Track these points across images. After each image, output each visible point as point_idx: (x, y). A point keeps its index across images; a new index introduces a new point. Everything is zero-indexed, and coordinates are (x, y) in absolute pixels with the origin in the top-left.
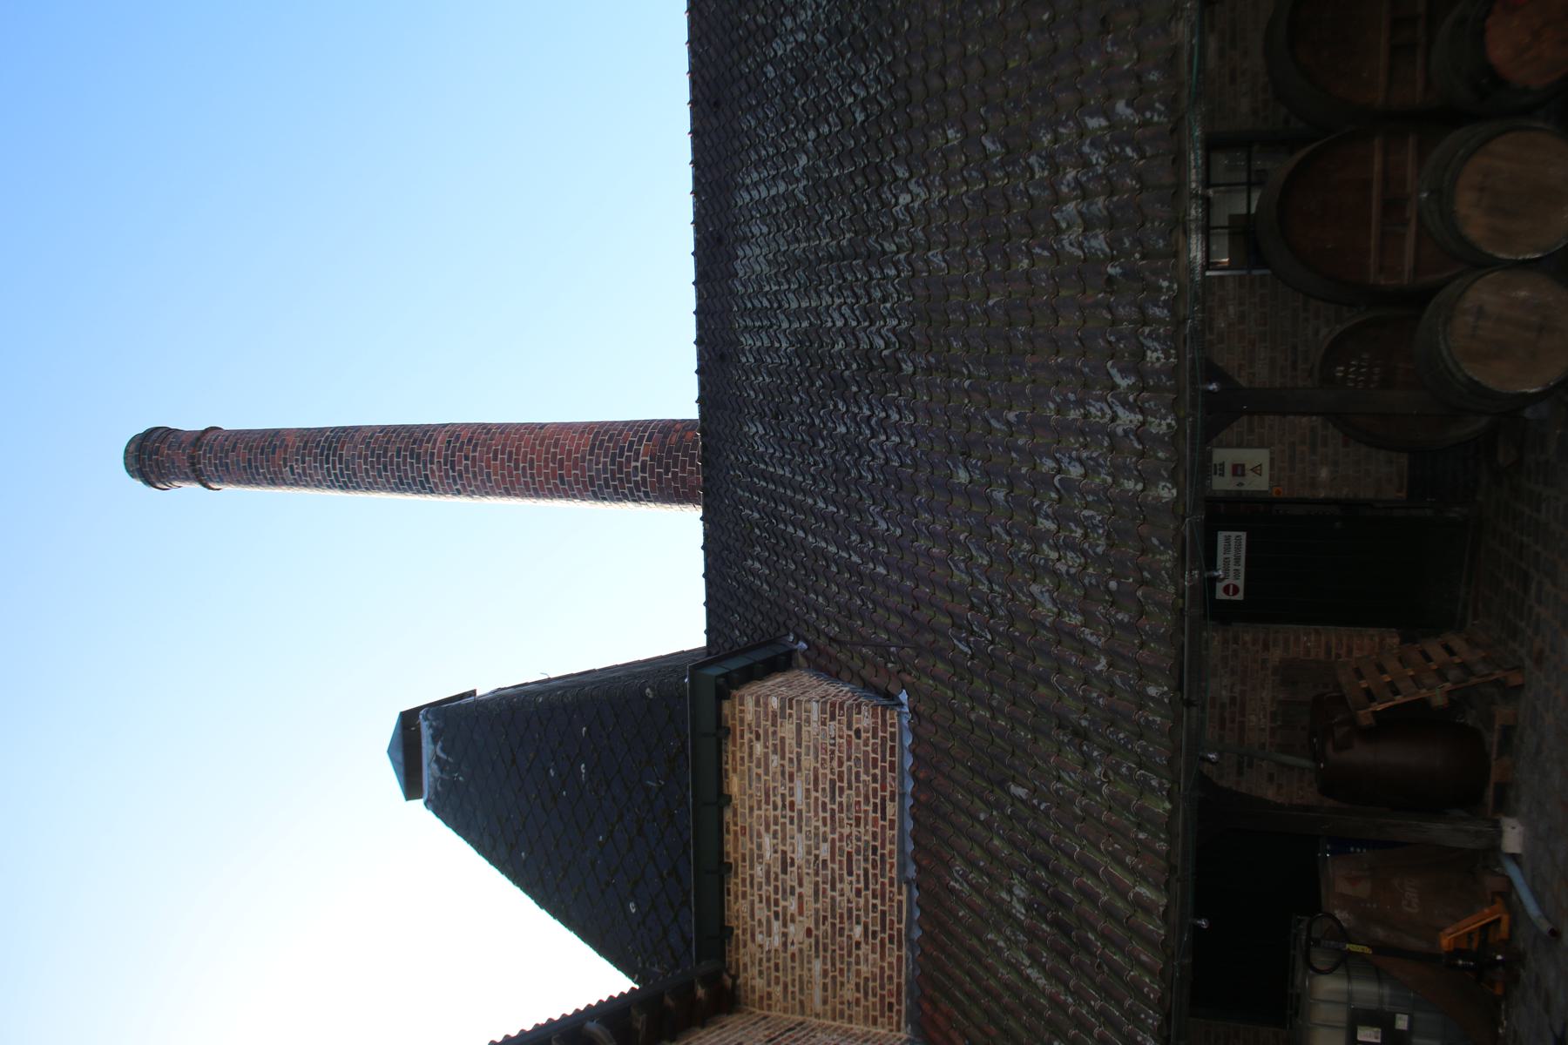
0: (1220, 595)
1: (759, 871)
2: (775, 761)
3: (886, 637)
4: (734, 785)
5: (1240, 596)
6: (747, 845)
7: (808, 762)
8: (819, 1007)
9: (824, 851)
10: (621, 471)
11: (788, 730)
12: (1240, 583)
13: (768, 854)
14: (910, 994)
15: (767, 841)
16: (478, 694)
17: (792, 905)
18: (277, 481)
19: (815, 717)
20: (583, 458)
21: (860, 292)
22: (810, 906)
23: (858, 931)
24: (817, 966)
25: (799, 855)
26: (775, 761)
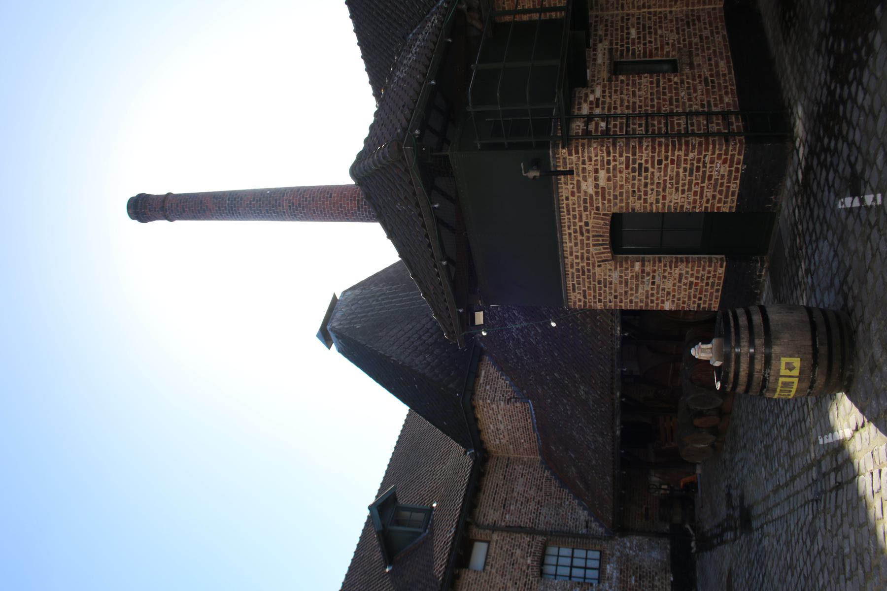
1: (490, 431)
2: (491, 412)
3: (521, 480)
4: (479, 416)
7: (502, 412)
9: (510, 427)
11: (494, 406)
15: (491, 426)
17: (501, 436)
24: (511, 447)
26: (491, 412)
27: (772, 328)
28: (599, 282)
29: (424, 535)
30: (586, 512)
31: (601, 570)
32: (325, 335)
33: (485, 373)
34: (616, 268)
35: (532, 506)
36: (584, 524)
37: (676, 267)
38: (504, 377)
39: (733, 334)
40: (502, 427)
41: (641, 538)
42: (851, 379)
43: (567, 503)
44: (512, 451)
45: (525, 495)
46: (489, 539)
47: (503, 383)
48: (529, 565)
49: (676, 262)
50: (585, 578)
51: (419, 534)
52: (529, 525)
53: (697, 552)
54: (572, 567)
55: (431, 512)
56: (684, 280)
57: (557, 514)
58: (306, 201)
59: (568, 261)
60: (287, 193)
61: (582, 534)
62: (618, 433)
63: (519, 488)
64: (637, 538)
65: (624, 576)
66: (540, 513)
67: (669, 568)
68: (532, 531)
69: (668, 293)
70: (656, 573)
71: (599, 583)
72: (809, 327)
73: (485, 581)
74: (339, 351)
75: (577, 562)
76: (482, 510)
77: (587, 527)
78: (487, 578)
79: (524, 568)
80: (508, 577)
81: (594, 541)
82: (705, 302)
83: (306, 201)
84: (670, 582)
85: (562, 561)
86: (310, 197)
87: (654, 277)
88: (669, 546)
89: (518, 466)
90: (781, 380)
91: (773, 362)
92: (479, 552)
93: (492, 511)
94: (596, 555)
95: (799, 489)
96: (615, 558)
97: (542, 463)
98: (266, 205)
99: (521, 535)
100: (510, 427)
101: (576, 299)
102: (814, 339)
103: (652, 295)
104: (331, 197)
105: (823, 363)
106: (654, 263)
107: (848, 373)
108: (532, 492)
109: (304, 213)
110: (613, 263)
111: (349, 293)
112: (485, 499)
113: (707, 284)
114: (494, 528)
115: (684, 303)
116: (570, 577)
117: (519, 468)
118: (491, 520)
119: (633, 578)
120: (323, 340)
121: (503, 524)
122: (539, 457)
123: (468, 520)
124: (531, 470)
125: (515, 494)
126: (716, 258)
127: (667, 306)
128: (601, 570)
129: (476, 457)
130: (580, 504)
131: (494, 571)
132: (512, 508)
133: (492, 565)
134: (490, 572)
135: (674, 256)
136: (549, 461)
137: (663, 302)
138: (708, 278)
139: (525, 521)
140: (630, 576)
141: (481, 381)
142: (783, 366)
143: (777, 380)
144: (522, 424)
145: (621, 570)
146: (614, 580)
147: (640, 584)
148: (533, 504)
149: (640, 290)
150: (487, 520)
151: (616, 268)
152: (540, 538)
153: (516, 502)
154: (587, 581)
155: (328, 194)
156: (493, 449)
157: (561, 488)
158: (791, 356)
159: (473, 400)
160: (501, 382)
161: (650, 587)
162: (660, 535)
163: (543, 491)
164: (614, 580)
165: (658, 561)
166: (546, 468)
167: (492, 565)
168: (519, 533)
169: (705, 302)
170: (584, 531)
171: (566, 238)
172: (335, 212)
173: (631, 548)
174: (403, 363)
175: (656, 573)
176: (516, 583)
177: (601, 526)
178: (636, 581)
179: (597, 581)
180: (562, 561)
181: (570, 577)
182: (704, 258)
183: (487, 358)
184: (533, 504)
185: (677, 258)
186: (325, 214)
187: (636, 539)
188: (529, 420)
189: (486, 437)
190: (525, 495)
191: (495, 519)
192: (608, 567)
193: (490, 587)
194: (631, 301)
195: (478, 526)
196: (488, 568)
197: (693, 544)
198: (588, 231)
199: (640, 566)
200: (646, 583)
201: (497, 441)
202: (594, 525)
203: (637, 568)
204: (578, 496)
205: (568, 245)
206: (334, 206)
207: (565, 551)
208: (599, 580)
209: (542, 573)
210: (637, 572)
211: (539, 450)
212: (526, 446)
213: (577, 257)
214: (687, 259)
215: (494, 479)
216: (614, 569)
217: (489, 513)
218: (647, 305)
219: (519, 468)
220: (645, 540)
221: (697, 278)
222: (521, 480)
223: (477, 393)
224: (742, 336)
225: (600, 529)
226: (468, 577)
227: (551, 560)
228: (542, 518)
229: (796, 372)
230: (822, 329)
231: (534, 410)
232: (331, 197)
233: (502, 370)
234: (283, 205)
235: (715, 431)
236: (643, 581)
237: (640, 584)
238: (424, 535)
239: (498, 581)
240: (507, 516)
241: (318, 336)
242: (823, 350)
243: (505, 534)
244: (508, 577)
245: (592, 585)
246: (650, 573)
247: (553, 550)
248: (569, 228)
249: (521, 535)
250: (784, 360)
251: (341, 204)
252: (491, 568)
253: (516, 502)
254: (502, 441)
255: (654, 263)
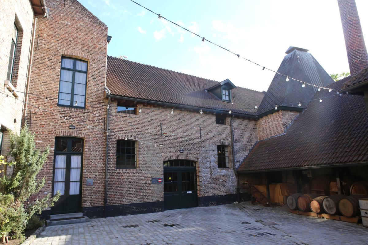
0: (303, 171)
1: (268, 120)
2: (277, 119)
3: (249, 134)
4: (274, 114)
5: (303, 174)
6: (269, 117)
7: (278, 123)
8: (259, 130)
9: (271, 127)
10: (352, 58)
11: (280, 119)
12: (304, 174)
13: (269, 120)
14: (262, 140)
15: (270, 120)
16: (308, 52)
17: (266, 125)
18: (36, 199)
19: (282, 122)
20: (352, 50)
21: (353, 111)
22: (266, 127)
23: (265, 133)
24: (262, 129)
25: (270, 124)
26: (277, 119)
32: (291, 50)
33: (292, 114)
36: (238, 160)
38: (292, 122)
40: (270, 124)
43: (244, 153)
47: (290, 122)
58: (354, 27)
60: (357, 18)
61: (235, 160)
65: (222, 177)
70: (225, 189)
73: (213, 125)
74: (285, 57)
76: (237, 120)
78: (214, 125)
79: (220, 139)
81: (233, 165)
83: (354, 27)
84: (223, 194)
86: (357, 28)
88: (235, 193)
89: (254, 133)
93: (237, 124)
95: (85, 243)
100: (271, 127)
104: (358, 37)
109: (348, 27)
111: (311, 56)
119: (222, 181)
120: (289, 49)
121: (233, 129)
122: (259, 141)
124: (254, 138)
131: (217, 128)
133: (219, 127)
134: (216, 126)
139: (236, 137)
140: (222, 179)
141: (289, 113)
144: (273, 132)
145: (224, 176)
147: (220, 183)
148: (242, 140)
153: (242, 133)
155: (360, 35)
156: (259, 122)
159: (282, 111)
160: (290, 121)
164: (221, 173)
167: (219, 127)
168: (231, 136)
172: (351, 40)
175: (225, 189)
176: (214, 136)
177: (238, 167)
183: (298, 114)
184: (242, 140)
186: (349, 36)
187: (235, 180)
188: (276, 134)
189: (264, 119)
192: (224, 171)
193: (211, 127)
195: (231, 120)
199: (226, 183)
200: (221, 186)
202: (238, 164)
203: (226, 182)
206: (354, 39)
210: (224, 182)
212: (263, 135)
215: (248, 124)
219: (253, 133)
223: (285, 112)
228: (238, 144)
232: (358, 37)
233: (295, 121)
234: (350, 17)
236: (221, 184)
237: (220, 183)
241: (290, 47)
243: (230, 130)
246: (225, 187)
251: (356, 42)
253: (242, 133)
254: (264, 125)
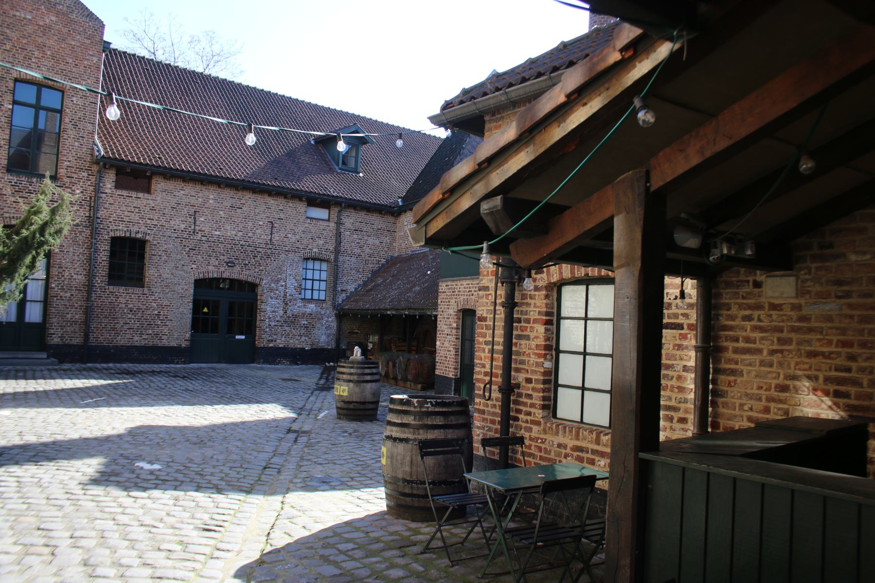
3: (377, 242)
27: (362, 384)
28: (449, 301)
29: (337, 168)
30: (353, 290)
31: (311, 300)
34: (454, 312)
35: (357, 251)
37: (454, 348)
39: (360, 366)
41: (335, 328)
42: (340, 418)
43: (360, 276)
44: (400, 234)
45: (365, 245)
46: (331, 220)
48: (312, 250)
49: (456, 349)
50: (305, 289)
51: (338, 165)
52: (342, 249)
53: (326, 366)
54: (313, 280)
55: (354, 172)
56: (448, 353)
57: (351, 269)
59: (459, 283)
62: (389, 313)
63: (371, 241)
64: (335, 326)
66: (352, 257)
67: (314, 347)
68: (337, 251)
69: (443, 344)
71: (301, 299)
72: (362, 401)
73: (299, 219)
75: (316, 284)
77: (342, 291)
79: (310, 247)
80: (303, 236)
82: (439, 366)
85: (317, 273)
87: (450, 335)
88: (330, 347)
90: (339, 387)
91: (346, 383)
92: (323, 213)
93: (352, 221)
94: (322, 297)
96: (320, 310)
97: (392, 257)
98: (600, 21)
99: (334, 244)
101: (443, 286)
102: (356, 402)
103: (443, 334)
105: (345, 406)
106: (456, 335)
107: (342, 417)
108: (368, 250)
110: (456, 310)
112: (362, 216)
113: (446, 367)
114: (339, 223)
115: (439, 353)
116: (306, 279)
117: (387, 240)
118: (345, 221)
119: (306, 323)
121: (342, 230)
122: (396, 255)
123: (343, 204)
124: (387, 249)
125: (366, 238)
126: (457, 372)
127: (438, 343)
128: (311, 300)
129: (394, 207)
130: (359, 285)
131: (307, 225)
132: (355, 236)
135: (460, 347)
136: (393, 261)
137: (440, 340)
138: (448, 367)
139: (345, 245)
142: (344, 388)
143: (339, 385)
145: (312, 314)
146: (304, 309)
149: (445, 327)
150: (345, 218)
151: (454, 312)
152: (332, 257)
154: (303, 291)
157: (259, 284)
158: (348, 392)
161: (300, 333)
162: (338, 342)
163: (369, 258)
164: (304, 309)
165: (319, 339)
166: (387, 260)
169: (439, 366)
170: (339, 289)
171: (468, 282)
173: (327, 321)
174: (463, 148)
176: (298, 241)
178: (304, 324)
179: (303, 297)
180: (317, 273)
181: (306, 279)
182: (458, 365)
184: (359, 251)
185: (459, 349)
187: (334, 325)
190: (365, 245)
191: (346, 224)
192: (314, 305)
194: (441, 321)
195: (340, 212)
196: (309, 221)
197: (332, 364)
198: (469, 296)
200: (303, 331)
201: (406, 223)
204: (365, 284)
205: (465, 283)
207: (324, 276)
208: (303, 299)
209: (307, 259)
211: (401, 255)
213: (460, 288)
214: (458, 355)
215: (377, 221)
216: (312, 309)
217: (351, 219)
218: (439, 331)
219: (387, 240)
220: (334, 330)
221: (449, 361)
222: (377, 242)
224: (359, 370)
225: (340, 300)
226: (301, 207)
227: (317, 265)
229: (341, 394)
230: (362, 407)
231: (421, 253)
235: (387, 375)
238: (337, 168)
239: (299, 228)
240: (348, 233)
242: (351, 406)
243: (334, 232)
244: (303, 236)
245: (300, 294)
246: (310, 334)
247: (324, 266)
248: (472, 284)
249: (334, 244)
250: (346, 388)
252: (309, 223)
255: (456, 335)
